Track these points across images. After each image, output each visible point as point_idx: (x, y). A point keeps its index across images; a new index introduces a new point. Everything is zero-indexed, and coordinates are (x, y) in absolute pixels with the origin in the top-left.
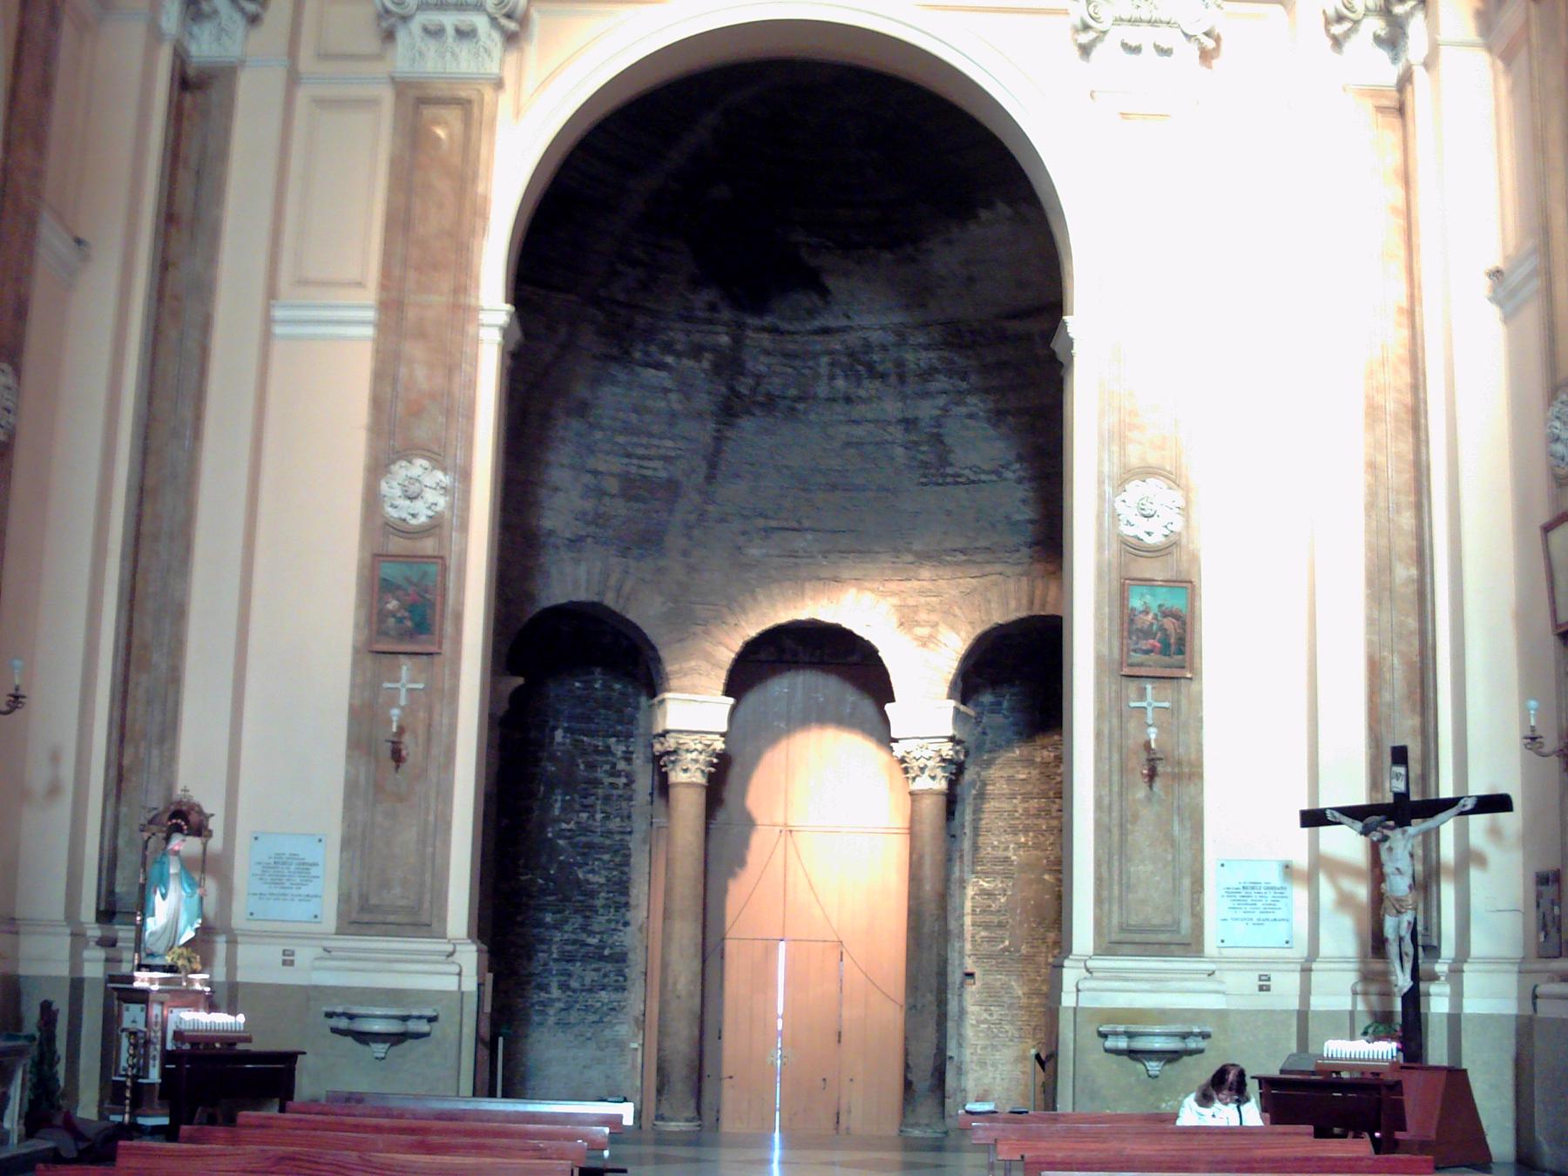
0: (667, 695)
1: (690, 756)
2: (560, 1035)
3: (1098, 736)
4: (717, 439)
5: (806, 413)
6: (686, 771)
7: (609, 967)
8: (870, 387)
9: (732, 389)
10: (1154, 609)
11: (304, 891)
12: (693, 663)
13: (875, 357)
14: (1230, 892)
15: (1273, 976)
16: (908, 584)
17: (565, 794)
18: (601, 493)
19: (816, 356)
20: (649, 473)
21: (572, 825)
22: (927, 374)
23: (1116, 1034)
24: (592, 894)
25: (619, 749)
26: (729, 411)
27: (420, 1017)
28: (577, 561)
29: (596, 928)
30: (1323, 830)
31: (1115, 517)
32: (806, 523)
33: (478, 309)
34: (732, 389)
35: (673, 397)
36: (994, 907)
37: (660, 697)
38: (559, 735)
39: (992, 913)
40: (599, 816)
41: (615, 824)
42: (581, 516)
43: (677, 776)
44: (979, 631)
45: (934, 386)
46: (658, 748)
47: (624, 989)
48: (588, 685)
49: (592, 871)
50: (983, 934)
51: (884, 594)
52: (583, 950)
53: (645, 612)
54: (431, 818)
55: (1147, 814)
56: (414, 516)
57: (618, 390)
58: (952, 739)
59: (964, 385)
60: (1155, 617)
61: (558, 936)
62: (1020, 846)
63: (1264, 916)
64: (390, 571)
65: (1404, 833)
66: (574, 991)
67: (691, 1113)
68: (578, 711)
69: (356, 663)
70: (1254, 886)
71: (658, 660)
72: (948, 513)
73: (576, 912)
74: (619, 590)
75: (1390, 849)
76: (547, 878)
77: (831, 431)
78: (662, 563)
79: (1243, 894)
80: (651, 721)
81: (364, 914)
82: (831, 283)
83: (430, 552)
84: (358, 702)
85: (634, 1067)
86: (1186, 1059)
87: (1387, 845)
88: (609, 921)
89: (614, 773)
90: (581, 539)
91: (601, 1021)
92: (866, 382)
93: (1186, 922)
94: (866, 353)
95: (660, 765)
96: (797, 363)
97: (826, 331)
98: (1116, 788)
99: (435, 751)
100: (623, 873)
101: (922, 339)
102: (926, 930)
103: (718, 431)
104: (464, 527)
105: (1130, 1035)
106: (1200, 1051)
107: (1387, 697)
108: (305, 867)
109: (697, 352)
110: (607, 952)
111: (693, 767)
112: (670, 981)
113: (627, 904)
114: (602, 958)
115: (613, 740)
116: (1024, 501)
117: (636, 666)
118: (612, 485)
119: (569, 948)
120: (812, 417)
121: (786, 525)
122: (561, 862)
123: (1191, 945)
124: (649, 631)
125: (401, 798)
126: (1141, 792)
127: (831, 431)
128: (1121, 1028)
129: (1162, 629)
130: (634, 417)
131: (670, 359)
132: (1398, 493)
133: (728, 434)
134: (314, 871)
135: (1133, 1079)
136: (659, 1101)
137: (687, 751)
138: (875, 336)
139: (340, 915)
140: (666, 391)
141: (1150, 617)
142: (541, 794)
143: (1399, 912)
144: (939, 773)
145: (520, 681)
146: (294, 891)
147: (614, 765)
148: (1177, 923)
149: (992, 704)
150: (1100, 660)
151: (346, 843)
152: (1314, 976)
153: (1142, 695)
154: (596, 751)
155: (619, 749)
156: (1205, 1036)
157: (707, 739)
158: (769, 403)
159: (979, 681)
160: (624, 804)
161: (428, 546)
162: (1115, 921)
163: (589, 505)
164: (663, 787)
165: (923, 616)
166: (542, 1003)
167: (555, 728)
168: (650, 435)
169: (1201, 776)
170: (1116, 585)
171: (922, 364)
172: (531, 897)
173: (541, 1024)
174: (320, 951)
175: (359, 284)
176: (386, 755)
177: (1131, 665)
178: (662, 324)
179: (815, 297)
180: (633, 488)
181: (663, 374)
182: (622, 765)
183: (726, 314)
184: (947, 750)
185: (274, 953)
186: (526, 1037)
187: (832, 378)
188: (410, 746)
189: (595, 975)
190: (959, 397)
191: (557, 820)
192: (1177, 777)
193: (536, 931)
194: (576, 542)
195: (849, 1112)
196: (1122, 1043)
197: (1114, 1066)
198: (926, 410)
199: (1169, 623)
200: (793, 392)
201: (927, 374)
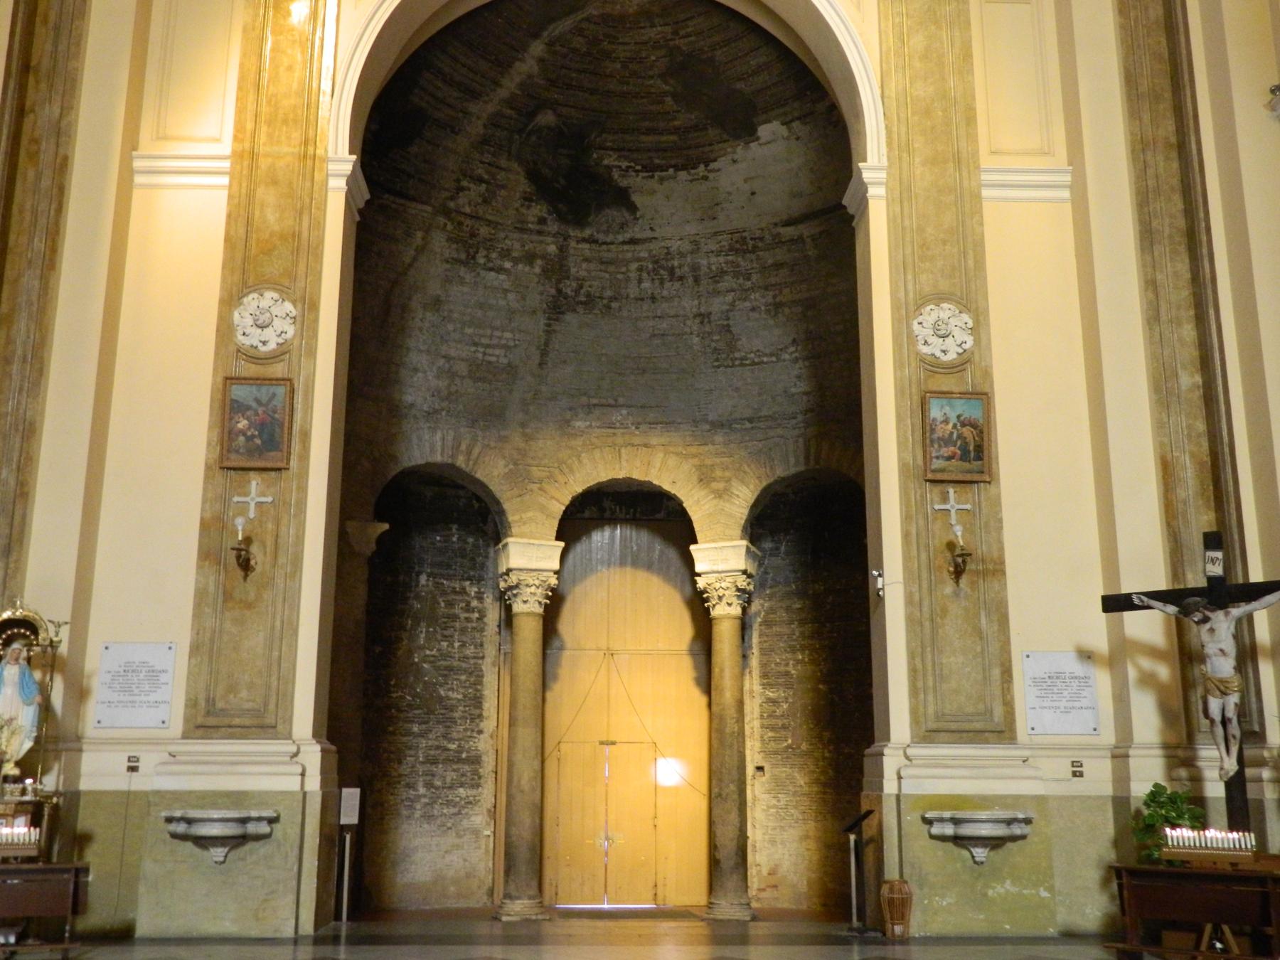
0: (510, 540)
1: (529, 590)
2: (426, 826)
3: (906, 536)
4: (548, 332)
5: (620, 309)
6: (525, 602)
7: (467, 768)
8: (671, 288)
9: (559, 291)
10: (953, 420)
11: (153, 697)
12: (530, 514)
13: (676, 263)
14: (1036, 682)
15: (1085, 762)
16: (706, 448)
17: (428, 626)
18: (452, 375)
19: (627, 262)
20: (493, 359)
21: (434, 652)
22: (718, 276)
23: (941, 820)
24: (452, 709)
25: (473, 590)
26: (557, 308)
27: (259, 819)
28: (433, 430)
29: (455, 735)
30: (1128, 615)
31: (912, 338)
32: (621, 400)
33: (325, 160)
34: (559, 291)
35: (511, 296)
36: (778, 712)
37: (504, 542)
38: (423, 579)
39: (777, 717)
40: (457, 645)
41: (470, 651)
42: (436, 393)
43: (518, 607)
44: (765, 484)
45: (723, 286)
46: (502, 585)
47: (478, 786)
48: (447, 539)
49: (452, 689)
50: (770, 734)
51: (686, 457)
52: (445, 755)
53: (492, 472)
54: (278, 623)
55: (955, 609)
56: (264, 343)
57: (466, 289)
58: (744, 572)
59: (748, 284)
60: (955, 426)
61: (423, 743)
62: (798, 662)
63: (1070, 704)
64: (241, 393)
65: (1227, 614)
66: (437, 788)
67: (533, 892)
68: (439, 559)
69: (208, 478)
70: (1059, 675)
71: (502, 513)
72: (737, 389)
73: (439, 722)
74: (469, 453)
75: (1212, 630)
76: (415, 696)
77: (640, 324)
78: (503, 433)
79: (1050, 683)
80: (496, 566)
81: (209, 720)
82: (637, 199)
83: (280, 376)
84: (208, 515)
85: (487, 851)
86: (1010, 845)
87: (1208, 626)
88: (466, 730)
89: (468, 609)
90: (436, 412)
91: (459, 813)
92: (668, 285)
93: (999, 711)
94: (667, 260)
95: (505, 600)
96: (612, 268)
97: (633, 241)
98: (925, 585)
99: (282, 560)
100: (477, 690)
101: (713, 246)
102: (728, 730)
103: (549, 325)
104: (312, 353)
105: (956, 822)
106: (1023, 837)
107: (1181, 493)
108: (154, 675)
109: (530, 258)
110: (464, 755)
111: (532, 599)
112: (515, 779)
113: (480, 716)
114: (460, 760)
115: (468, 583)
116: (798, 377)
117: (484, 521)
118: (462, 368)
119: (432, 752)
120: (625, 313)
121: (604, 401)
122: (425, 682)
123: (1004, 732)
124: (494, 487)
125: (249, 606)
126: (949, 588)
127: (640, 324)
128: (947, 814)
129: (960, 436)
130: (479, 313)
131: (508, 265)
132: (1179, 308)
133: (557, 328)
134: (163, 678)
135: (958, 865)
136: (506, 882)
137: (527, 586)
138: (675, 245)
139: (187, 720)
140: (506, 291)
141: (950, 426)
142: (409, 627)
143: (1224, 694)
144: (736, 601)
145: (386, 526)
146: (143, 698)
147: (468, 604)
148: (989, 712)
149: (771, 549)
150: (904, 469)
151: (195, 649)
152: (1133, 762)
153: (945, 499)
154: (454, 592)
155: (473, 590)
156: (1028, 821)
157: (543, 576)
158: (590, 302)
159: (761, 531)
160: (477, 635)
161: (278, 370)
162: (931, 710)
163: (442, 384)
164: (508, 619)
165: (718, 473)
166: (409, 799)
167: (419, 574)
168: (494, 328)
169: (1003, 573)
170: (916, 399)
171: (714, 268)
172: (399, 710)
173: (409, 817)
174: (166, 757)
175: (217, 140)
176: (235, 561)
177: (933, 471)
178: (502, 235)
179: (627, 215)
180: (480, 371)
181: (502, 277)
182: (475, 603)
183: (553, 227)
184: (742, 582)
185: (119, 761)
186: (396, 828)
187: (640, 281)
188: (258, 555)
189: (454, 775)
190: (744, 293)
191: (422, 648)
192: (984, 574)
193: (405, 739)
194: (431, 414)
195: (665, 885)
196: (949, 830)
197: (940, 853)
198: (717, 305)
199: (967, 431)
200: (608, 293)
201: (718, 276)
